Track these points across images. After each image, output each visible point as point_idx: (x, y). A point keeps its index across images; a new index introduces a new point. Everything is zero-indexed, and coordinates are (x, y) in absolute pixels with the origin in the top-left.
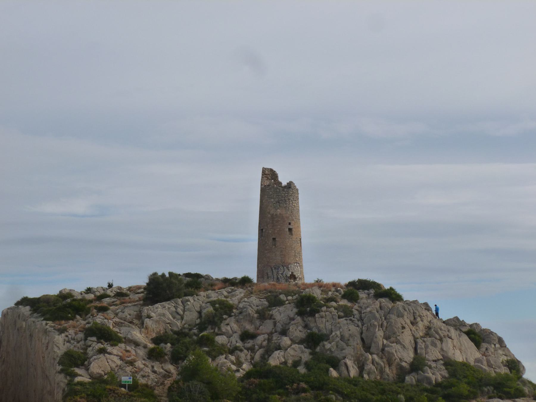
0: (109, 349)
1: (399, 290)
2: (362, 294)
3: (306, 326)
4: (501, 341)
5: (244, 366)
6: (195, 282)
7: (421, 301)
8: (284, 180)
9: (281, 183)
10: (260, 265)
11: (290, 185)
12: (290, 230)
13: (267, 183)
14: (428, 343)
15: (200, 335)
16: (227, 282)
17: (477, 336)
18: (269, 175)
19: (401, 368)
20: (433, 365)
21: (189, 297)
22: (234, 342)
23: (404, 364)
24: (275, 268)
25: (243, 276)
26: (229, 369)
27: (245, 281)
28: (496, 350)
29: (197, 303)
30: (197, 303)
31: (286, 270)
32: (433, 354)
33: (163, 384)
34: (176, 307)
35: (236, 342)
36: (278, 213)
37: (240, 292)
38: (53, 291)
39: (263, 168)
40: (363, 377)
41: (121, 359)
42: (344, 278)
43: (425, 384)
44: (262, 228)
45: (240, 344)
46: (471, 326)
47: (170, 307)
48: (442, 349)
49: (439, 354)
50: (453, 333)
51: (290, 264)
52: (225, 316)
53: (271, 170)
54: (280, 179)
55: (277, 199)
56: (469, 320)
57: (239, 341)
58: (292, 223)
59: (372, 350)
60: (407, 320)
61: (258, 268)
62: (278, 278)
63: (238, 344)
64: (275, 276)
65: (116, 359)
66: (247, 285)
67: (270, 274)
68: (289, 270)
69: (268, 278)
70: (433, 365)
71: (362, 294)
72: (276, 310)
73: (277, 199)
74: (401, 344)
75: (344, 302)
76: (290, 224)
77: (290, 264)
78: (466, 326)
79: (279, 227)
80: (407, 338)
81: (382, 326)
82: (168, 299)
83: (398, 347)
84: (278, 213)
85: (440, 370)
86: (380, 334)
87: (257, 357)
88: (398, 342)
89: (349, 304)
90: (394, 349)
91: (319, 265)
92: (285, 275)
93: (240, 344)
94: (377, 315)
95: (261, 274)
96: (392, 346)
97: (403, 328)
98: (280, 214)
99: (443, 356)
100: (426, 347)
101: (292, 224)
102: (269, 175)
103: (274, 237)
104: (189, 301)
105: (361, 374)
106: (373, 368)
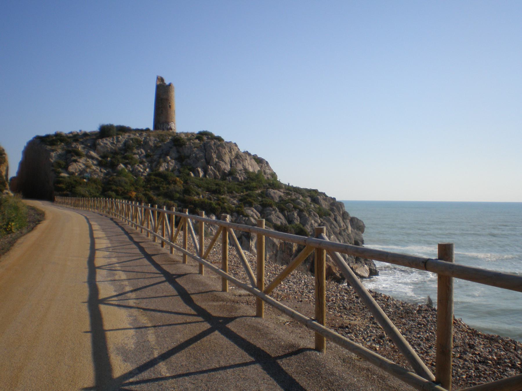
0: (79, 160)
3: (178, 152)
4: (267, 163)
5: (148, 170)
6: (122, 130)
7: (233, 142)
8: (167, 82)
11: (170, 85)
13: (159, 83)
14: (237, 162)
15: (255, 289)
16: (137, 130)
19: (225, 173)
20: (240, 172)
23: (226, 171)
26: (140, 171)
27: (147, 130)
28: (265, 167)
29: (123, 138)
30: (123, 138)
32: (240, 167)
33: (295, 208)
34: (113, 140)
38: (52, 132)
40: (206, 177)
41: (84, 164)
42: (196, 131)
48: (243, 165)
50: (248, 158)
55: (163, 96)
60: (227, 150)
65: (81, 165)
66: (148, 132)
70: (240, 172)
73: (163, 96)
80: (227, 158)
81: (215, 152)
82: (108, 137)
83: (223, 163)
85: (243, 175)
86: (214, 156)
88: (223, 161)
90: (222, 164)
91: (186, 121)
94: (213, 147)
95: (156, 127)
97: (225, 154)
100: (236, 164)
105: (205, 175)
106: (211, 173)
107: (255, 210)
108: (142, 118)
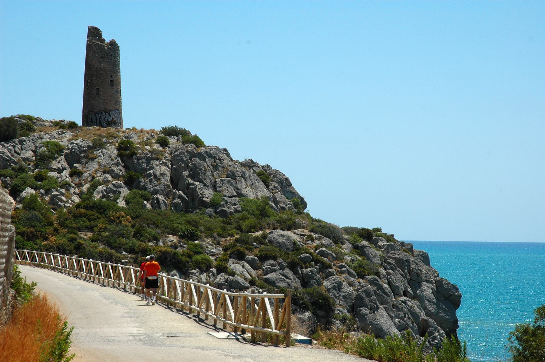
1: (202, 138)
2: (172, 141)
7: (221, 147)
8: (107, 37)
9: (104, 40)
12: (112, 81)
17: (266, 175)
18: (94, 33)
22: (64, 178)
24: (98, 114)
25: (73, 121)
27: (72, 126)
36: (102, 67)
37: (68, 134)
39: (89, 27)
45: (69, 180)
46: (263, 167)
49: (234, 192)
51: (111, 110)
53: (96, 28)
54: (104, 37)
55: (102, 63)
56: (261, 162)
57: (68, 176)
58: (114, 76)
59: (179, 186)
61: (83, 113)
62: (100, 123)
63: (67, 179)
67: (94, 119)
68: (110, 116)
71: (172, 141)
73: (102, 63)
75: (156, 146)
76: (111, 76)
77: (111, 110)
78: (259, 167)
84: (102, 67)
87: (85, 188)
89: (161, 149)
91: (142, 111)
92: (106, 120)
93: (69, 180)
95: (88, 119)
99: (237, 192)
102: (94, 33)
103: (98, 87)
104: (25, 141)
107: (246, 265)
108: (56, 97)
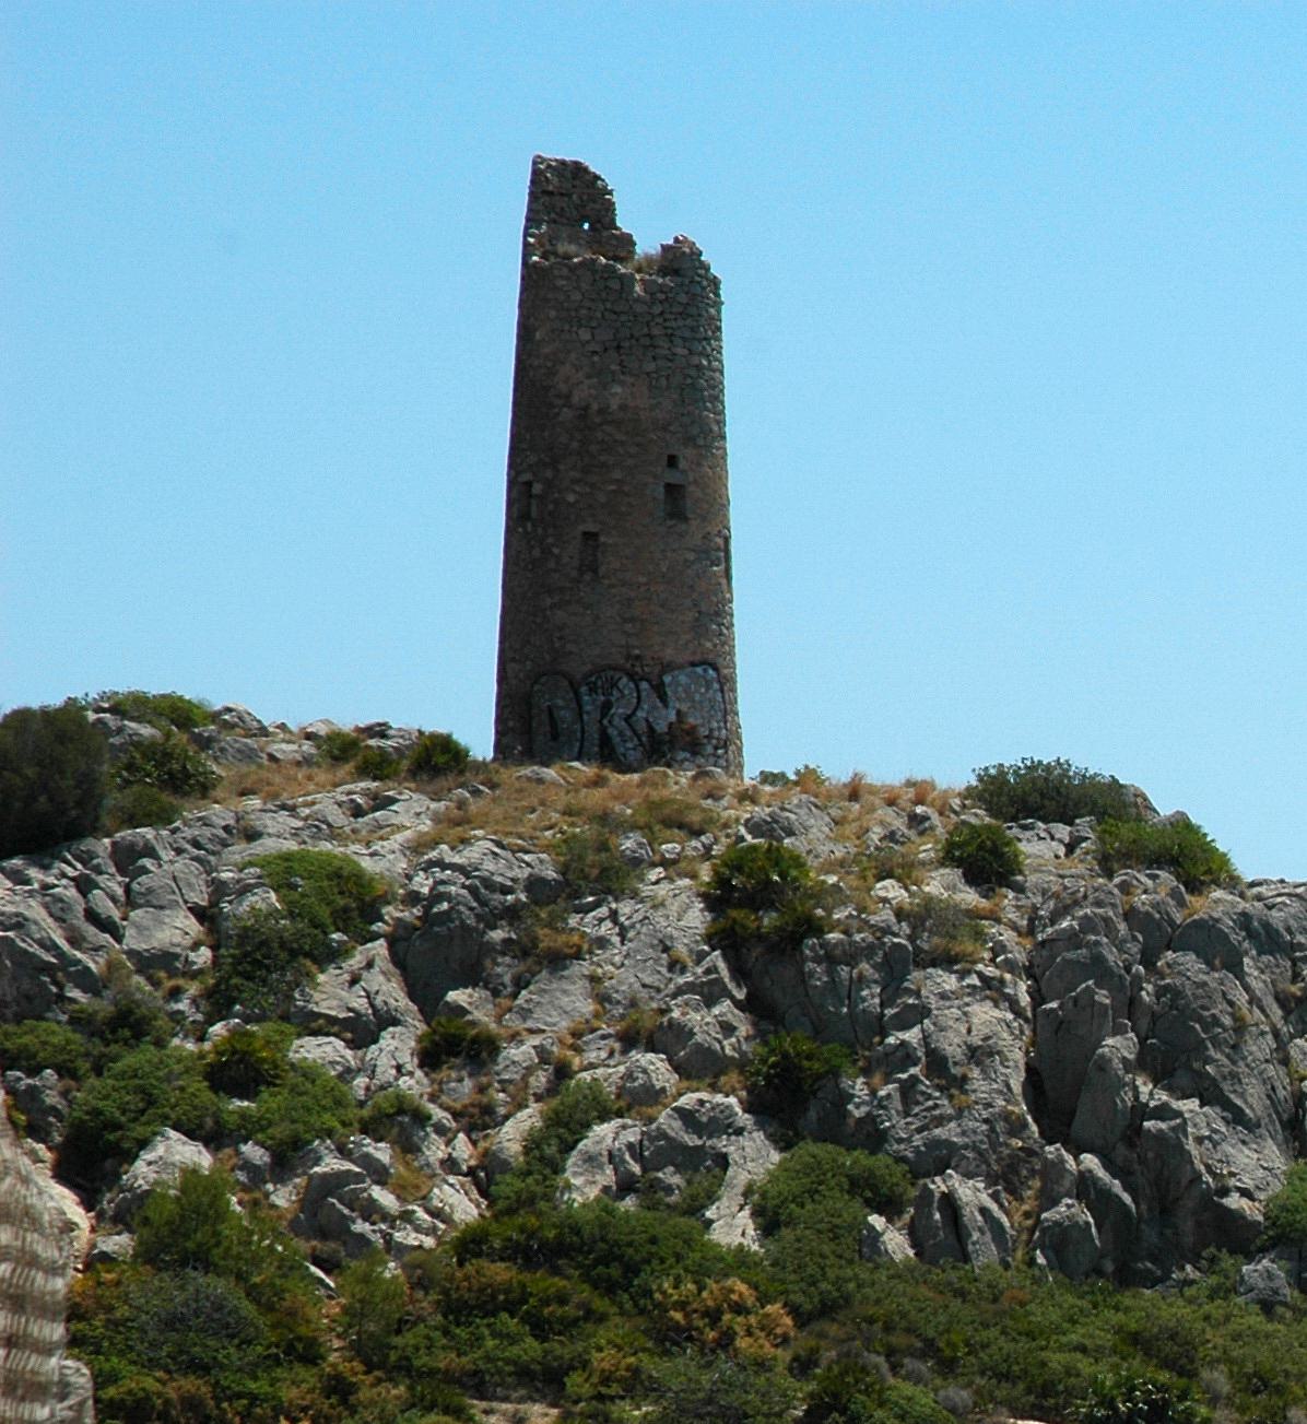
2: (1039, 849)
8: (646, 225)
9: (627, 241)
10: (511, 667)
12: (673, 491)
18: (567, 200)
21: (148, 833)
22: (386, 1072)
24: (592, 690)
27: (435, 759)
31: (650, 698)
34: (84, 885)
35: (399, 1068)
36: (614, 404)
37: (413, 812)
39: (537, 161)
43: (334, 936)
44: (526, 477)
47: (51, 880)
52: (923, 1149)
55: (614, 383)
57: (411, 1063)
58: (686, 456)
62: (605, 740)
64: (593, 731)
68: (663, 698)
69: (555, 737)
72: (603, 911)
73: (614, 383)
74: (1226, 1105)
75: (942, 884)
76: (672, 461)
79: (617, 475)
84: (614, 404)
89: (970, 897)
92: (642, 727)
95: (528, 721)
96: (1179, 1114)
98: (623, 407)
101: (682, 464)
102: (567, 200)
103: (591, 527)
104: (150, 852)
